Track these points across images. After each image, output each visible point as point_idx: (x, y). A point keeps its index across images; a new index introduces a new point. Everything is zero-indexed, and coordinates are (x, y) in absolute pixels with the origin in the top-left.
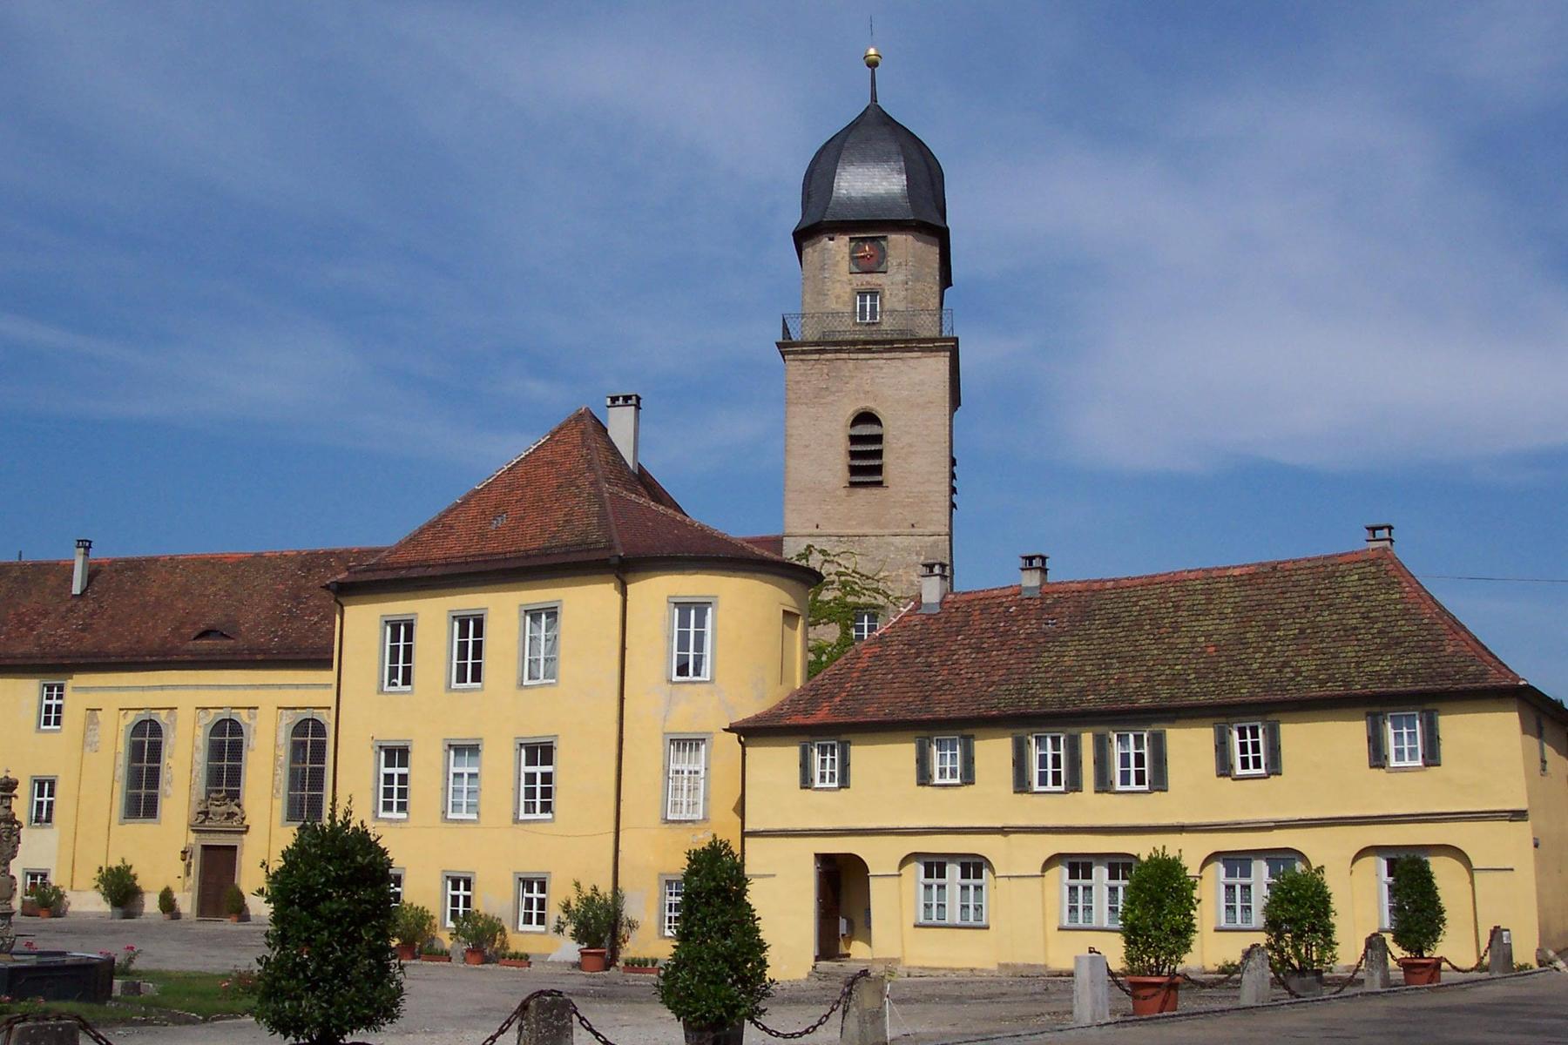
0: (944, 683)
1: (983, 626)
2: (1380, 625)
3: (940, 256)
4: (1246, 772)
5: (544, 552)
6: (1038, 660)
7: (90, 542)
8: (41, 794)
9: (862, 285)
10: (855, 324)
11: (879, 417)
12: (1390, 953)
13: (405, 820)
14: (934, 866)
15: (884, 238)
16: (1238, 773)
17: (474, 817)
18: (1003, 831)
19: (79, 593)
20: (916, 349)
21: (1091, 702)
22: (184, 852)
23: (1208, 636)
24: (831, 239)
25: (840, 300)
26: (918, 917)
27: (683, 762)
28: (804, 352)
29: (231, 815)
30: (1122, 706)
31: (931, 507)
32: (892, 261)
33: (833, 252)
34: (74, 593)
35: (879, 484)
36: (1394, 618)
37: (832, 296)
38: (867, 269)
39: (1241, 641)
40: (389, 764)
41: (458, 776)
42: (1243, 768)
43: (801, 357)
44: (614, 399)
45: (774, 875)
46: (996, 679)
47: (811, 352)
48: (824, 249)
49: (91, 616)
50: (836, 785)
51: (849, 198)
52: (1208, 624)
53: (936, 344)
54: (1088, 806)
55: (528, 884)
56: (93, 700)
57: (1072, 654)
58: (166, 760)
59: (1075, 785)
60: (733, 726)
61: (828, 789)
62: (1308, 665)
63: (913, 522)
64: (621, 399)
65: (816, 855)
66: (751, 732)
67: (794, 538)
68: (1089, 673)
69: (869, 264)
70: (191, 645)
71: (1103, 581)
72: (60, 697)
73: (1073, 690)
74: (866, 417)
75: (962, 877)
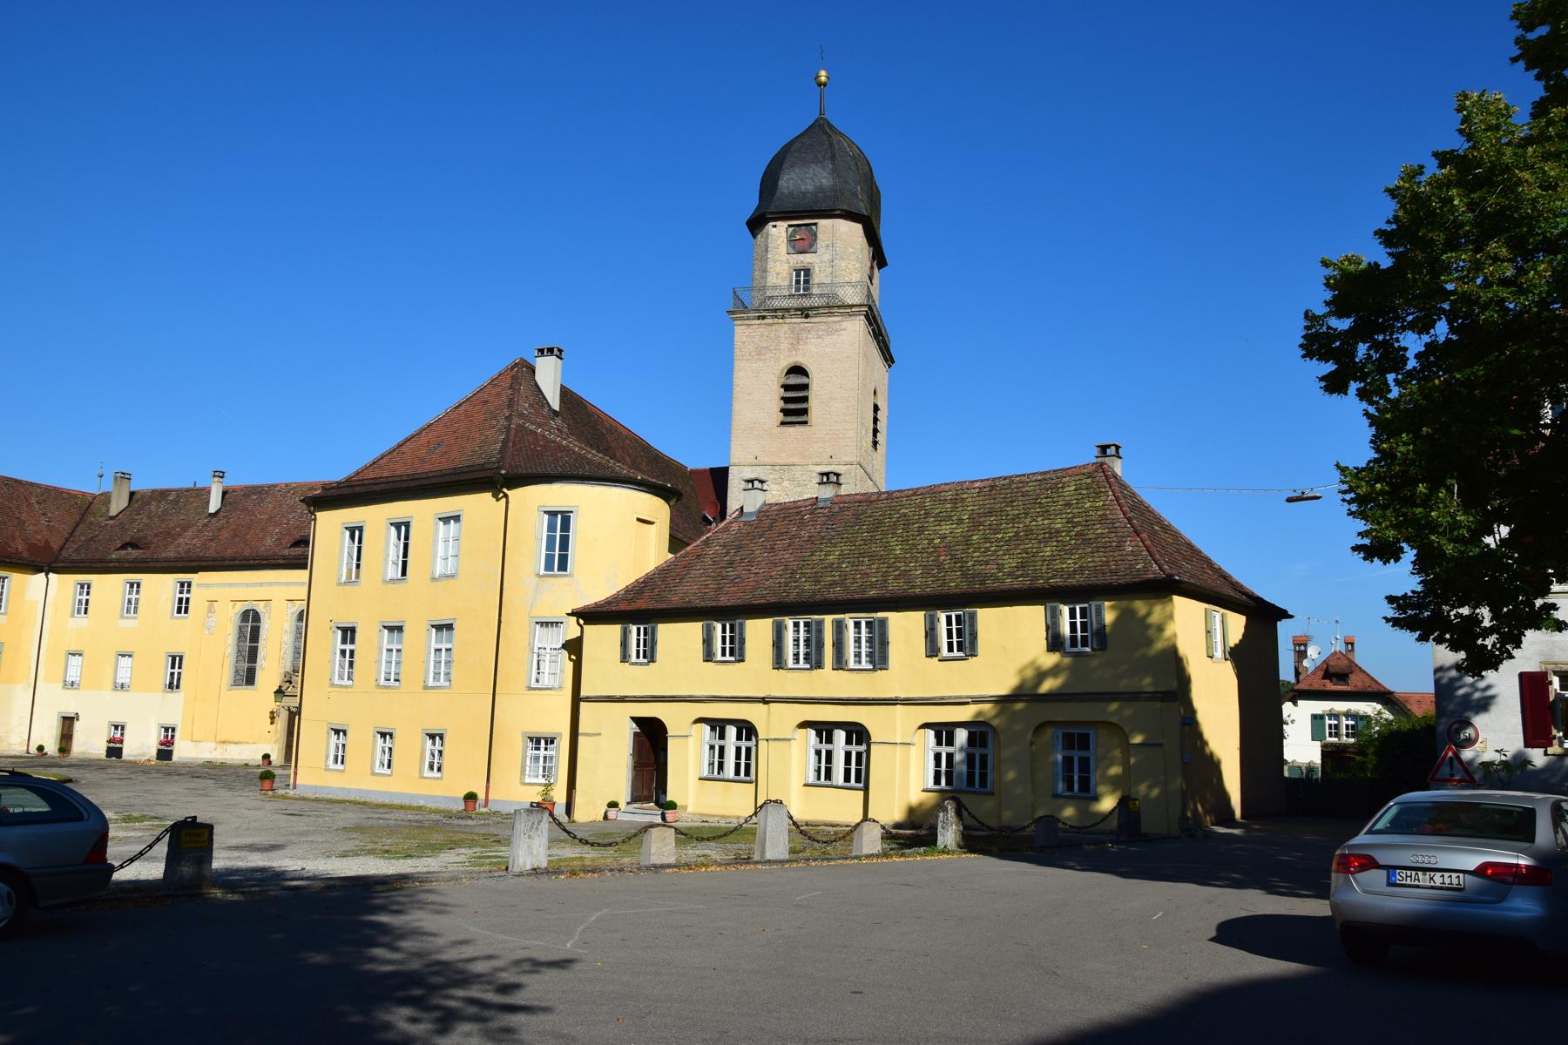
1: (781, 531)
2: (1079, 528)
4: (951, 654)
5: (470, 469)
7: (223, 473)
12: (966, 810)
13: (351, 687)
16: (944, 655)
18: (764, 701)
19: (213, 512)
20: (837, 314)
21: (837, 593)
23: (943, 538)
26: (806, 777)
32: (821, 242)
34: (210, 512)
36: (1092, 522)
38: (801, 250)
39: (967, 541)
41: (390, 650)
42: (949, 651)
43: (747, 322)
44: (541, 351)
45: (599, 734)
46: (773, 574)
49: (219, 530)
52: (945, 528)
54: (827, 681)
56: (212, 593)
57: (837, 553)
62: (1010, 563)
63: (831, 454)
69: (803, 243)
70: (286, 552)
72: (188, 591)
74: (797, 370)
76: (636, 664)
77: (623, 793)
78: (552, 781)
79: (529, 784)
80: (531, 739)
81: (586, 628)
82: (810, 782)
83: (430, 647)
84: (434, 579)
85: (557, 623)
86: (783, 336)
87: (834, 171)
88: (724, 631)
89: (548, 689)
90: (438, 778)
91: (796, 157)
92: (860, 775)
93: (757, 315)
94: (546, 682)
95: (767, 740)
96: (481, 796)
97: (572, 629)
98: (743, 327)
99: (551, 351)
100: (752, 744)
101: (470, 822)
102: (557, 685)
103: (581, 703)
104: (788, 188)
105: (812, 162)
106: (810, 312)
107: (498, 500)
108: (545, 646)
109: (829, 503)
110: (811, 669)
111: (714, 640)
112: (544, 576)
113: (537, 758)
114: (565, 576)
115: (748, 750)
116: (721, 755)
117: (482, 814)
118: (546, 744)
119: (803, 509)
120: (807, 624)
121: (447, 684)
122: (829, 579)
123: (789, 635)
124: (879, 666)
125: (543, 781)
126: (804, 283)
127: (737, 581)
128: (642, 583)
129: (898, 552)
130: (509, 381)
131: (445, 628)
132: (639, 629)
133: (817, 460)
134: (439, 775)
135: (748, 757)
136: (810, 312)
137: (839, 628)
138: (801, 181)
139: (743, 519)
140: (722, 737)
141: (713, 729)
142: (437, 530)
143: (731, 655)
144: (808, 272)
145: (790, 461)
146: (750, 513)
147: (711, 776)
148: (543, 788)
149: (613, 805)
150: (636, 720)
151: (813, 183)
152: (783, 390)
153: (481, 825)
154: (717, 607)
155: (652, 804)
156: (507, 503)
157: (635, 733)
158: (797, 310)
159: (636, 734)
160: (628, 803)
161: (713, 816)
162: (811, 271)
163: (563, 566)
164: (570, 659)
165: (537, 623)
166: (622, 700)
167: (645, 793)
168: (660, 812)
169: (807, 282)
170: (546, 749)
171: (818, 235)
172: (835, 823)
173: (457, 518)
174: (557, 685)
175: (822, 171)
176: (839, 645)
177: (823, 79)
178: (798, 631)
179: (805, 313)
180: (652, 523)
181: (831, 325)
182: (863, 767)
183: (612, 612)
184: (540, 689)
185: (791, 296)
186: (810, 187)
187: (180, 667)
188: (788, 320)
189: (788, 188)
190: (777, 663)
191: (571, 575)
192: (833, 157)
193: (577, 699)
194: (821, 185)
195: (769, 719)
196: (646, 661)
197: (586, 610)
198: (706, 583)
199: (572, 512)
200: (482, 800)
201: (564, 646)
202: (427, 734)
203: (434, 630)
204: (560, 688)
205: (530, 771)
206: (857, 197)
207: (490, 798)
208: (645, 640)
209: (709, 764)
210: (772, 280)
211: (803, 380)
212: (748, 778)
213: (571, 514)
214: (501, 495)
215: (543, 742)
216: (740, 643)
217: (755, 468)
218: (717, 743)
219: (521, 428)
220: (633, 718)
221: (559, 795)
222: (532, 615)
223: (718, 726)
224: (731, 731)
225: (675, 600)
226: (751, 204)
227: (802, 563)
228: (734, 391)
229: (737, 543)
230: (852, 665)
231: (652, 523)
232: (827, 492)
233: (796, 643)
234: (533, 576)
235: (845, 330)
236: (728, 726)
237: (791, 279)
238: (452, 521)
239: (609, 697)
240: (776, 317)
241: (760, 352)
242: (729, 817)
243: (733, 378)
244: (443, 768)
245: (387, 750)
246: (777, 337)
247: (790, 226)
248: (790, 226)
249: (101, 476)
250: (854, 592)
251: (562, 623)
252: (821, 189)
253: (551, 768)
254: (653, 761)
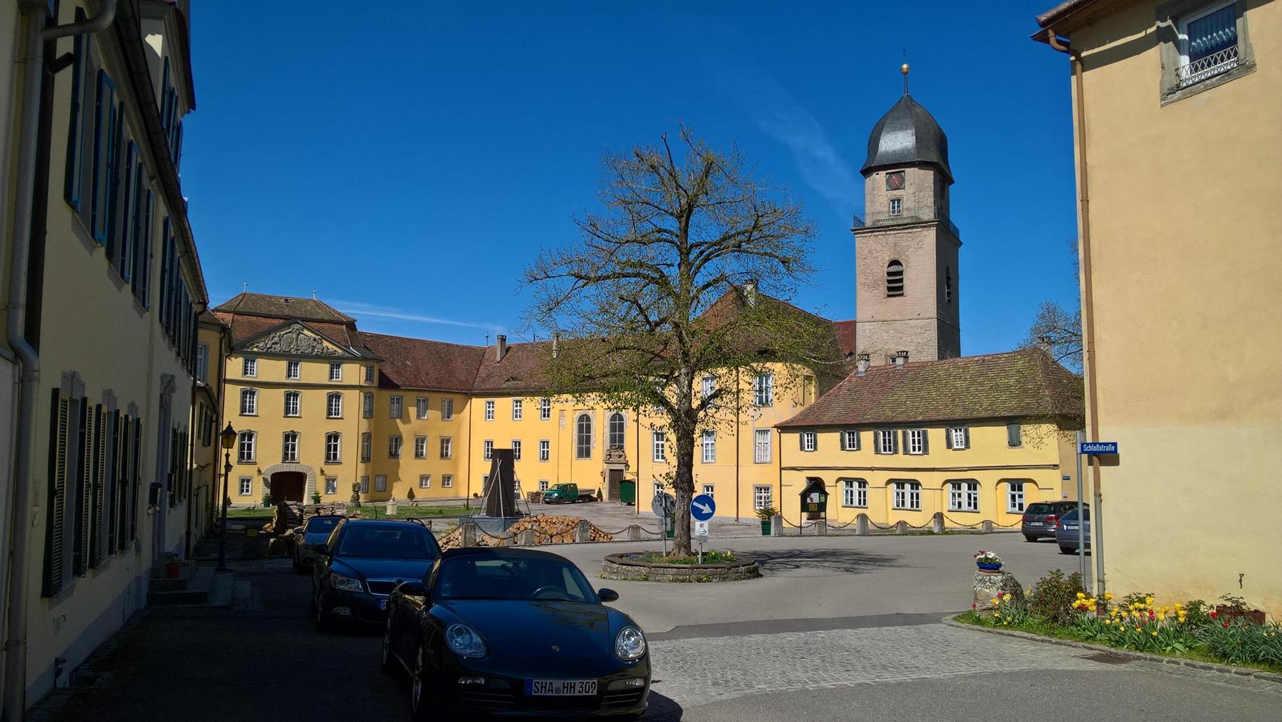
8: (544, 448)
10: (890, 216)
14: (956, 484)
17: (713, 461)
18: (871, 469)
21: (901, 418)
22: (602, 473)
26: (894, 505)
27: (760, 438)
28: (864, 233)
29: (620, 456)
32: (907, 183)
35: (902, 295)
40: (658, 440)
43: (863, 235)
47: (867, 232)
48: (874, 179)
50: (813, 449)
51: (887, 152)
52: (958, 383)
54: (900, 460)
55: (759, 489)
58: (592, 434)
59: (896, 452)
61: (810, 451)
62: (986, 403)
65: (807, 478)
66: (784, 428)
92: (916, 505)
98: (861, 238)
116: (903, 497)
121: (713, 461)
133: (910, 317)
145: (894, 318)
187: (547, 448)
207: (739, 516)
223: (849, 482)
225: (825, 420)
230: (912, 452)
248: (887, 174)
249: (487, 337)
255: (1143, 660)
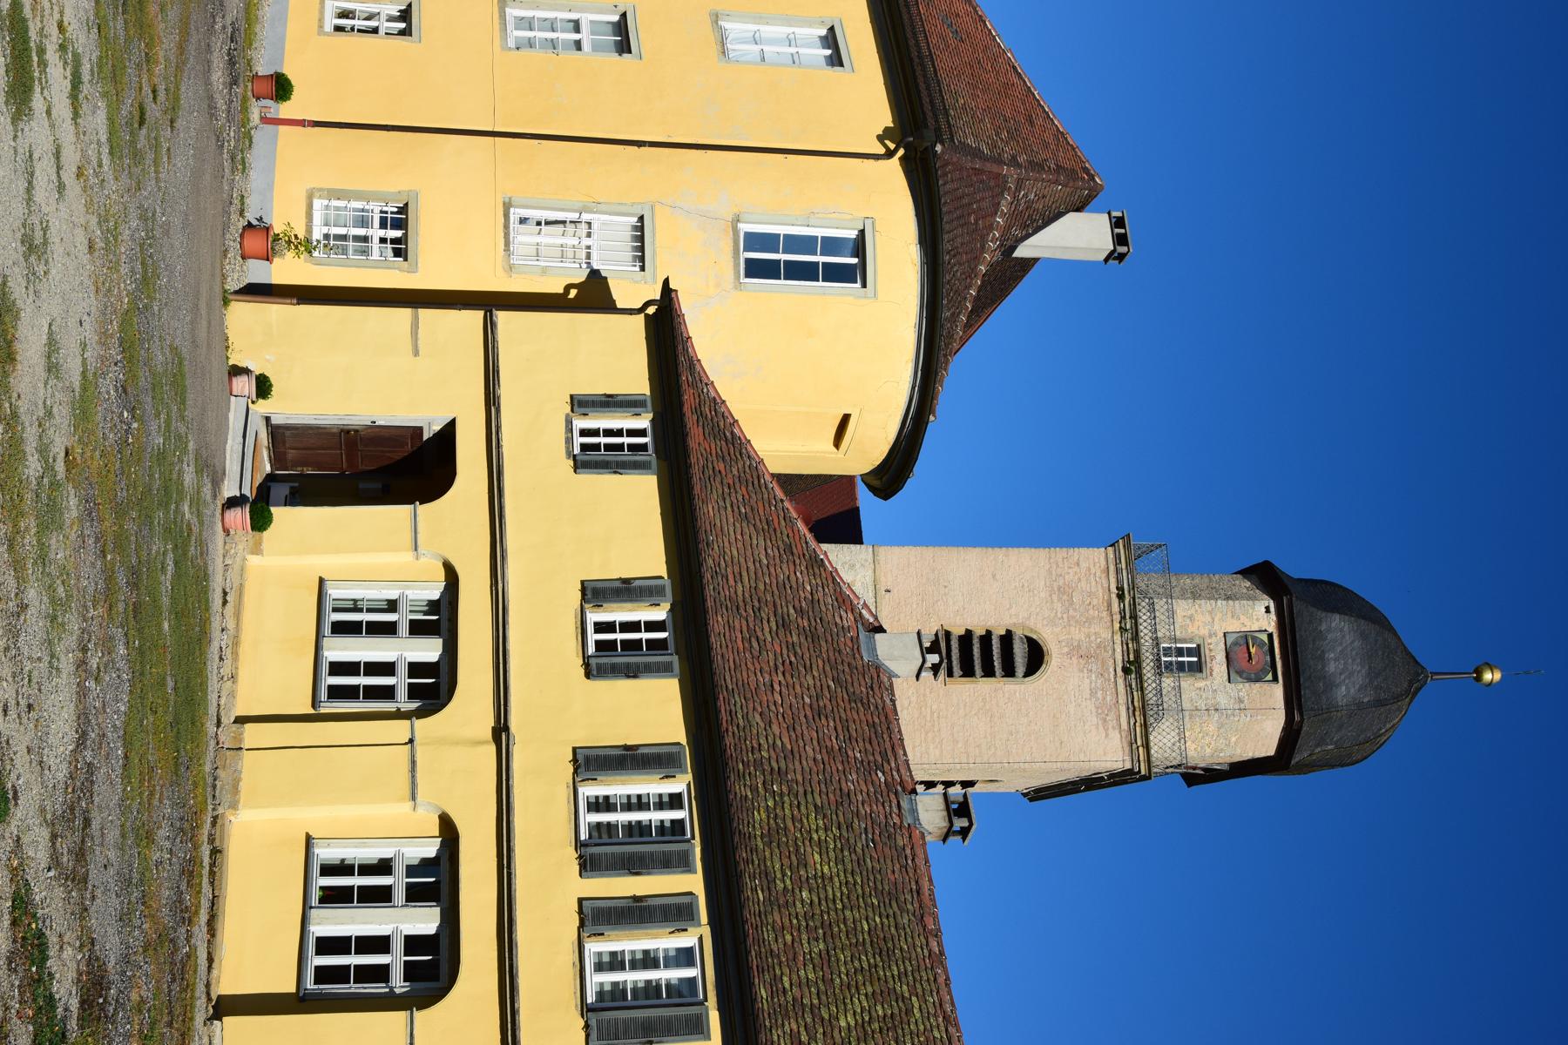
0: (762, 643)
1: (851, 723)
3: (1249, 761)
6: (812, 808)
9: (1211, 650)
11: (1035, 676)
15: (1275, 679)
18: (501, 731)
24: (1268, 610)
25: (1188, 621)
28: (1118, 571)
30: (753, 953)
31: (920, 745)
32: (1245, 689)
33: (1251, 611)
37: (1193, 611)
38: (1232, 655)
43: (1112, 568)
45: (416, 353)
46: (775, 728)
53: (1141, 749)
55: (399, 219)
57: (826, 869)
59: (589, 865)
60: (673, 295)
64: (1122, 231)
67: (871, 560)
68: (798, 897)
71: (937, 934)
73: (769, 863)
74: (1036, 657)
75: (408, 938)
76: (570, 429)
77: (287, 407)
78: (316, 254)
79: (310, 207)
80: (404, 210)
81: (640, 320)
82: (317, 851)
83: (581, 10)
84: (716, 18)
85: (642, 259)
86: (1092, 630)
87: (1360, 706)
88: (652, 626)
89: (507, 244)
90: (321, 27)
91: (1376, 641)
93: (1126, 586)
94: (520, 238)
95: (411, 741)
96: (286, 110)
97: (632, 290)
98: (1103, 563)
99: (1121, 240)
100: (403, 702)
101: (218, 77)
102: (515, 260)
103: (481, 313)
104: (1329, 630)
105: (1370, 667)
106: (1133, 676)
107: (881, 138)
108: (594, 236)
109: (910, 821)
110: (579, 844)
111: (629, 605)
112: (735, 231)
113: (363, 222)
114: (738, 277)
115: (387, 693)
117: (245, 109)
118: (394, 241)
119: (893, 765)
120: (678, 825)
121: (511, 43)
122: (777, 866)
123: (651, 786)
124: (593, 1023)
125: (317, 234)
126: (1178, 662)
127: (755, 644)
128: (732, 433)
129: (843, 1024)
130: (1067, 165)
131: (622, 37)
132: (642, 433)
134: (328, 27)
135: (374, 693)
136: (1133, 676)
137: (675, 912)
138: (1342, 651)
139: (863, 635)
140: (417, 629)
141: (433, 606)
142: (809, 23)
143: (600, 645)
144: (1197, 668)
146: (874, 649)
147: (328, 606)
148: (301, 236)
149: (263, 387)
150: (449, 432)
151: (1338, 671)
152: (1003, 633)
153: (211, 98)
154: (705, 612)
155: (268, 469)
156: (876, 157)
157: (420, 429)
158: (1137, 653)
159: (418, 431)
160: (268, 419)
161: (238, 615)
162: (1199, 675)
163: (756, 269)
164: (568, 288)
165: (641, 219)
166: (492, 400)
167: (291, 454)
168: (246, 491)
169: (1181, 666)
170: (383, 240)
171: (1258, 685)
172: (219, 926)
173: (836, 60)
174: (515, 260)
175: (1357, 687)
176: (637, 913)
177: (1488, 676)
178: (660, 805)
179: (1132, 667)
180: (837, 443)
181: (1114, 710)
182: (353, 988)
183: (678, 376)
184: (506, 226)
185: (1156, 641)
186: (1332, 667)
188: (1118, 638)
189: (1329, 630)
190: (587, 759)
191: (738, 285)
192: (1379, 703)
193: (489, 303)
194: (1338, 686)
195: (457, 743)
196: (577, 450)
197: (672, 319)
198: (744, 574)
199: (864, 285)
200: (277, 111)
201: (595, 274)
202: (410, 5)
203: (616, 18)
204: (510, 268)
205: (337, 209)
206: (1318, 745)
207: (282, 129)
208: (620, 447)
209: (355, 601)
210: (1182, 608)
211: (1020, 667)
212: (323, 694)
213: (858, 285)
214: (892, 146)
215: (398, 234)
216: (628, 665)
217: (871, 588)
218: (402, 618)
219: (1000, 184)
220: (452, 423)
221: (287, 270)
222: (658, 208)
224: (429, 650)
225: (711, 510)
226: (1293, 567)
227: (801, 790)
228: (997, 550)
229: (821, 630)
230: (594, 947)
231: (837, 443)
232: (930, 812)
233: (634, 800)
234: (736, 210)
235: (1107, 735)
236: (440, 641)
237: (1185, 641)
238: (829, 52)
239: (496, 372)
240: (1123, 618)
241: (1064, 592)
242: (235, 655)
243: (1019, 547)
244: (341, 37)
245: (373, 23)
246: (1089, 621)
247: (1270, 636)
248: (1270, 636)
250: (761, 942)
251: (643, 269)
252: (1330, 686)
253: (345, 251)
254: (362, 467)
255: (217, 782)
